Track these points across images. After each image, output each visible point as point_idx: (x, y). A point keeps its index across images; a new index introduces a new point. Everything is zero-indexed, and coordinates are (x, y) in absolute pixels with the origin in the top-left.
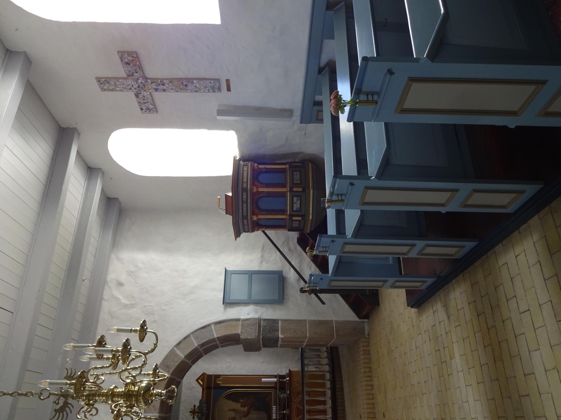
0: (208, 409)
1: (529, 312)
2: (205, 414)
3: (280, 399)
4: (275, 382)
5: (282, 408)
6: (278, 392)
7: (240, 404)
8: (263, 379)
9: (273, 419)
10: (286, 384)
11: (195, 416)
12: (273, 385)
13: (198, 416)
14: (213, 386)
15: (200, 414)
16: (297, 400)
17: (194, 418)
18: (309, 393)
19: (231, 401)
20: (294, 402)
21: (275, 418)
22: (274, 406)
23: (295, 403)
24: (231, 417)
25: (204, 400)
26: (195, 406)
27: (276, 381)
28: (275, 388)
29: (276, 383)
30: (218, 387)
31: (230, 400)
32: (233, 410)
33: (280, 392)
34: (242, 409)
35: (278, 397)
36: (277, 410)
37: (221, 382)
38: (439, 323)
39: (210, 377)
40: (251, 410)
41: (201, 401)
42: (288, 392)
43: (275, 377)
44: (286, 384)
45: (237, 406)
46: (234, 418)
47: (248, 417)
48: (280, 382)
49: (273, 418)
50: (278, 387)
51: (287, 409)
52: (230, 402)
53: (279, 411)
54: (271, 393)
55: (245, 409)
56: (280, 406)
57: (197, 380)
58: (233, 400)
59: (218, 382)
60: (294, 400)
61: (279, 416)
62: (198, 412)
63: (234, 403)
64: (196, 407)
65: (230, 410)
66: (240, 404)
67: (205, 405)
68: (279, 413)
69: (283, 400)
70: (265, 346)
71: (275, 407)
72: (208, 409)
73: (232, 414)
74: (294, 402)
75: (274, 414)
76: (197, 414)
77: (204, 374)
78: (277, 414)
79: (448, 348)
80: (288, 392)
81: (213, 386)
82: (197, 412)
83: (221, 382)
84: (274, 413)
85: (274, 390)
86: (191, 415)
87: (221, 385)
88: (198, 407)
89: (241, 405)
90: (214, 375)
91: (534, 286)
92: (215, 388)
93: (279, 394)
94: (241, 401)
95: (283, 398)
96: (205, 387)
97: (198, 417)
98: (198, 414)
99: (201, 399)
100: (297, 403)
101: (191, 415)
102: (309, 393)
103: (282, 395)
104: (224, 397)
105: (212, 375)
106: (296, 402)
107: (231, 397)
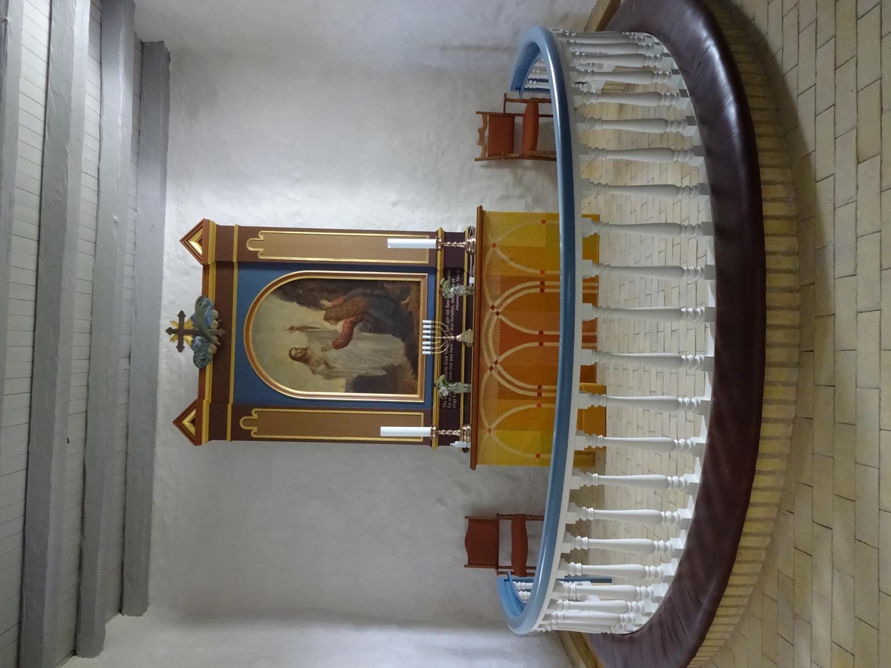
0: (224, 322)
1: (879, 311)
2: (215, 338)
3: (444, 301)
4: (431, 250)
5: (450, 327)
6: (440, 280)
7: (324, 312)
8: (390, 241)
9: (423, 355)
10: (466, 255)
11: (185, 344)
12: (426, 262)
13: (193, 342)
14: (235, 260)
15: (198, 338)
16: (501, 304)
17: (180, 348)
18: (542, 283)
19: (295, 304)
20: (493, 307)
21: (429, 353)
22: (425, 321)
23: (495, 310)
24: (296, 349)
25: (211, 297)
26: (182, 315)
27: (434, 247)
28: (430, 270)
29: (433, 252)
30: (251, 263)
31: (292, 300)
32: (302, 329)
33: (446, 279)
34: (328, 326)
35: (440, 292)
36: (437, 332)
37: (261, 250)
38: (817, 149)
39: (224, 232)
40: (356, 329)
41: (199, 300)
42: (472, 280)
43: (432, 235)
44: (466, 255)
45: (314, 317)
46: (306, 349)
47: (349, 347)
48: (446, 250)
49: (424, 352)
50: (439, 268)
51: (466, 330)
52: (292, 308)
53: (443, 335)
54: (419, 283)
55: (340, 327)
56: (444, 321)
57: (185, 241)
58: (303, 301)
59: (250, 249)
60: (490, 303)
61: (443, 349)
62: (193, 333)
63: (304, 309)
64: (186, 319)
65: (292, 329)
66: (324, 312)
67: (216, 312)
68: (443, 340)
69: (455, 303)
70: (646, 57)
71: (429, 322)
72: (224, 322)
73: (299, 341)
74: (493, 307)
75: (424, 343)
76: (189, 338)
77: (204, 225)
78: (436, 343)
79: (881, 233)
80: (472, 280)
81: (235, 260)
82: (187, 330)
83: (261, 250)
84: (427, 340)
85: (427, 274)
86: (172, 340)
87: (261, 257)
88: (192, 318)
89: (325, 316)
90: (239, 226)
91: (679, 286)
92: (242, 265)
93: (441, 286)
94: (326, 303)
95: (455, 296)
96: (211, 261)
97: (193, 345)
98: (194, 337)
99: (200, 294)
100: (500, 310)
101: (172, 340)
102: (542, 283)
103: (452, 289)
104: (273, 292)
105: (232, 228)
106: (499, 307)
107: (289, 292)
